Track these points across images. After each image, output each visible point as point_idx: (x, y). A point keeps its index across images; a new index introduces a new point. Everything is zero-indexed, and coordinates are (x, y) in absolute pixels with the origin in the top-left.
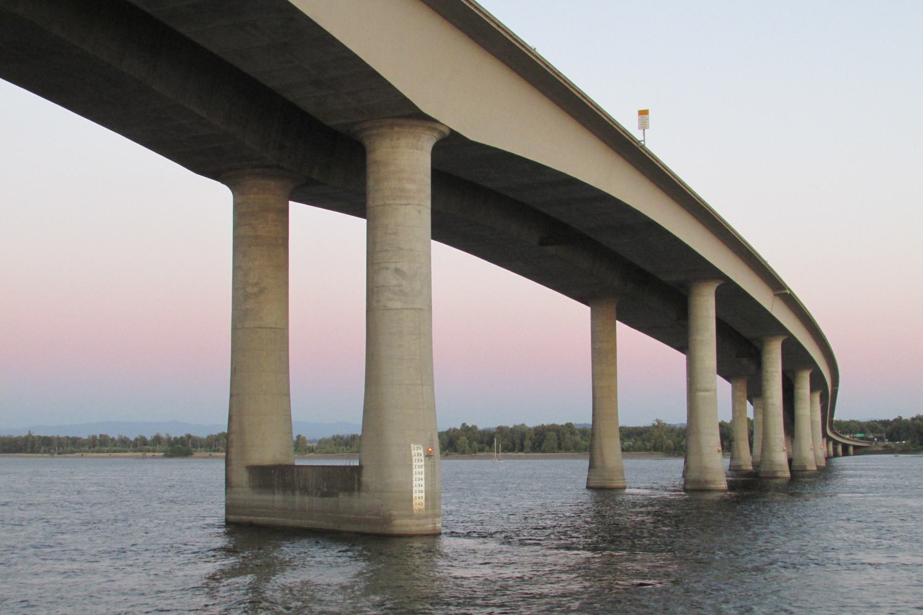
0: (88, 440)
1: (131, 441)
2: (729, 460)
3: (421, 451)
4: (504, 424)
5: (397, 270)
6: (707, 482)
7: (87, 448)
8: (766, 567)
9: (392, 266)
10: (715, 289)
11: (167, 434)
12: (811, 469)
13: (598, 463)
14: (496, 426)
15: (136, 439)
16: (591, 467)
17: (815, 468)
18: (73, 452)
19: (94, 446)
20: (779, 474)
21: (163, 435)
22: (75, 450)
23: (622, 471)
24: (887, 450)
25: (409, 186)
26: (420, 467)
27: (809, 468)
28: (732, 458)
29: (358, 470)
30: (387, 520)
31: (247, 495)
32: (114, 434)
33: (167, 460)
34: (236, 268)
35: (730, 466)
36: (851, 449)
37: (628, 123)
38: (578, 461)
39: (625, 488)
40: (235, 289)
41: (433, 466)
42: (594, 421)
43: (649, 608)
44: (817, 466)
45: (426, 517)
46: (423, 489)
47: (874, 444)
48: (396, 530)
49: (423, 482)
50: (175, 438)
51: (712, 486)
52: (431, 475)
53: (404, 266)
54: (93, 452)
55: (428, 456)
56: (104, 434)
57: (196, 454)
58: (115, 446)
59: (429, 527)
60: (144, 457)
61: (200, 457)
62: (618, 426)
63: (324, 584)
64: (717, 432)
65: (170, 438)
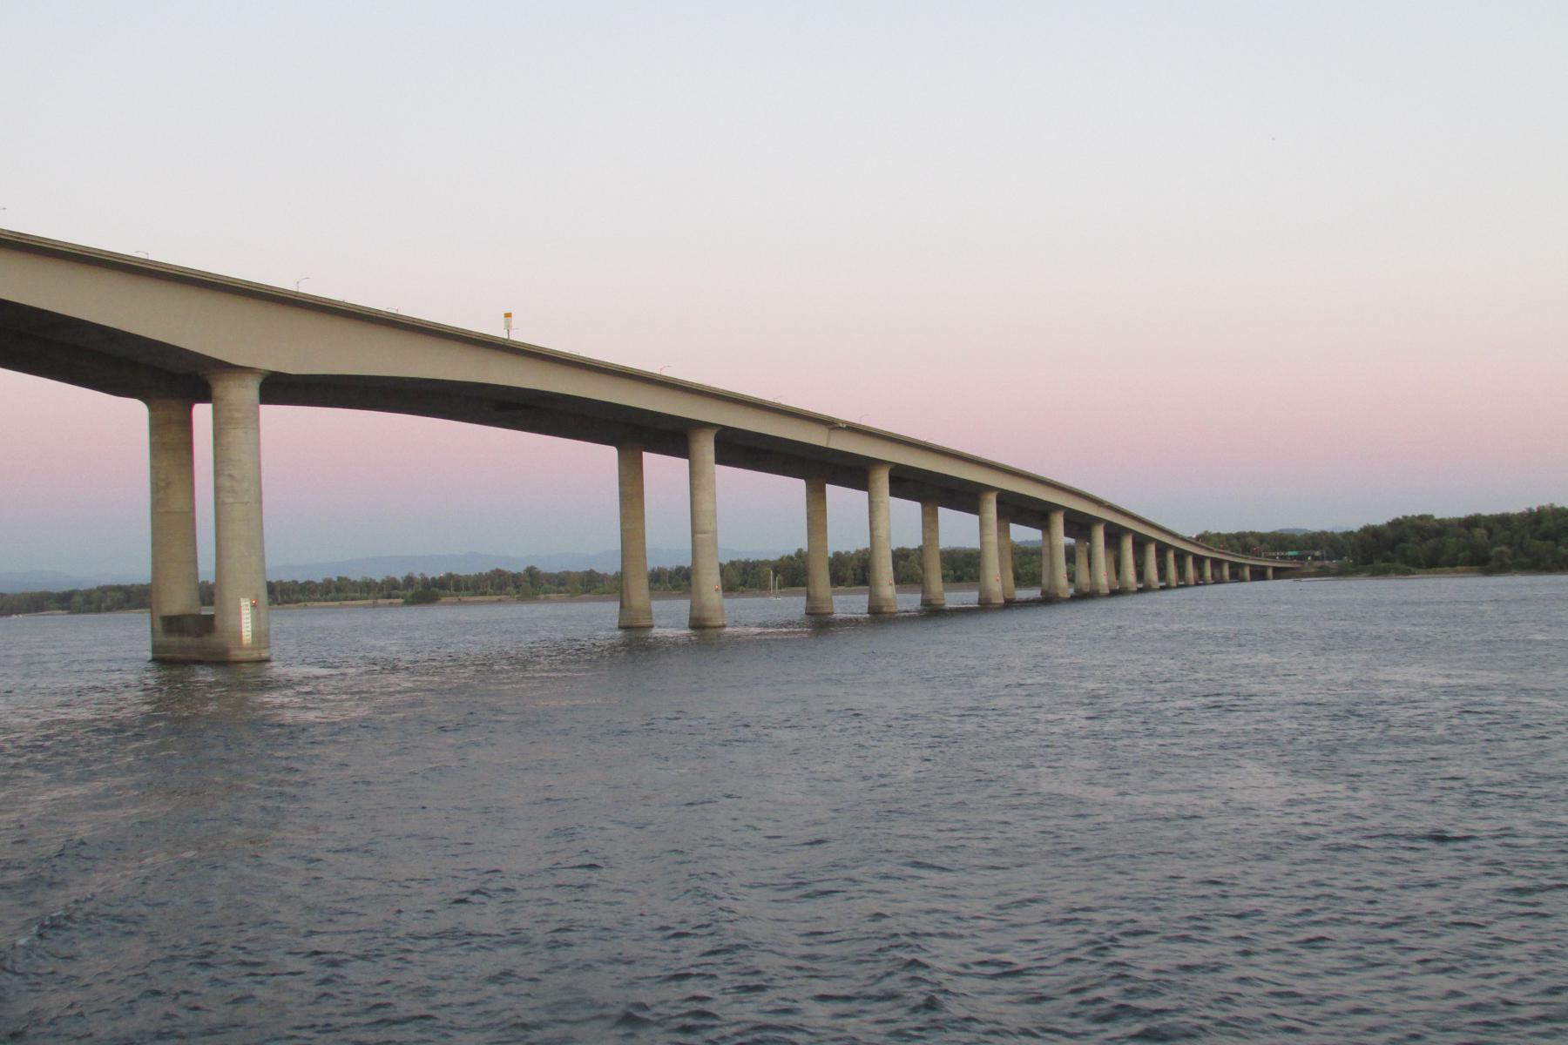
0: (321, 584)
1: (377, 583)
2: (920, 595)
3: (248, 603)
4: (1373, 523)
5: (231, 476)
6: (704, 619)
7: (319, 596)
8: (539, 685)
9: (226, 473)
10: (712, 438)
11: (422, 574)
12: (996, 602)
13: (626, 604)
14: (1216, 532)
15: (383, 582)
16: (622, 607)
17: (1002, 601)
18: (298, 601)
19: (328, 592)
20: (885, 609)
21: (417, 575)
22: (303, 598)
23: (649, 612)
24: (1323, 573)
25: (238, 415)
26: (248, 614)
27: (994, 601)
28: (923, 592)
29: (211, 617)
30: (226, 651)
31: (164, 639)
32: (356, 576)
33: (407, 608)
34: (152, 467)
35: (980, 599)
36: (1270, 572)
37: (497, 330)
38: (795, 599)
39: (652, 627)
40: (152, 483)
41: (258, 613)
42: (622, 569)
43: (920, 758)
44: (1005, 599)
45: (253, 649)
46: (250, 629)
47: (1307, 564)
48: (233, 658)
49: (249, 625)
50: (433, 579)
51: (709, 623)
52: (256, 620)
53: (235, 473)
54: (326, 600)
55: (254, 606)
56: (343, 576)
57: (444, 600)
58: (356, 591)
59: (255, 655)
60: (375, 606)
61: (445, 604)
62: (646, 568)
63: (1421, 832)
64: (717, 571)
65: (427, 579)
